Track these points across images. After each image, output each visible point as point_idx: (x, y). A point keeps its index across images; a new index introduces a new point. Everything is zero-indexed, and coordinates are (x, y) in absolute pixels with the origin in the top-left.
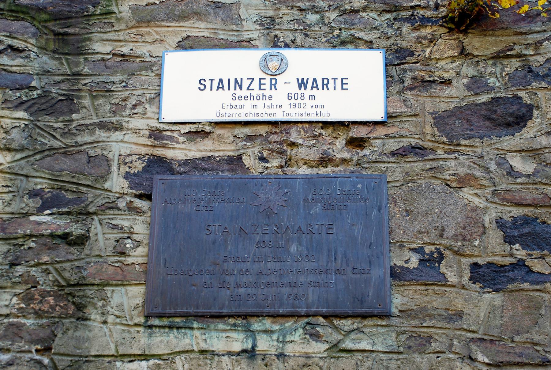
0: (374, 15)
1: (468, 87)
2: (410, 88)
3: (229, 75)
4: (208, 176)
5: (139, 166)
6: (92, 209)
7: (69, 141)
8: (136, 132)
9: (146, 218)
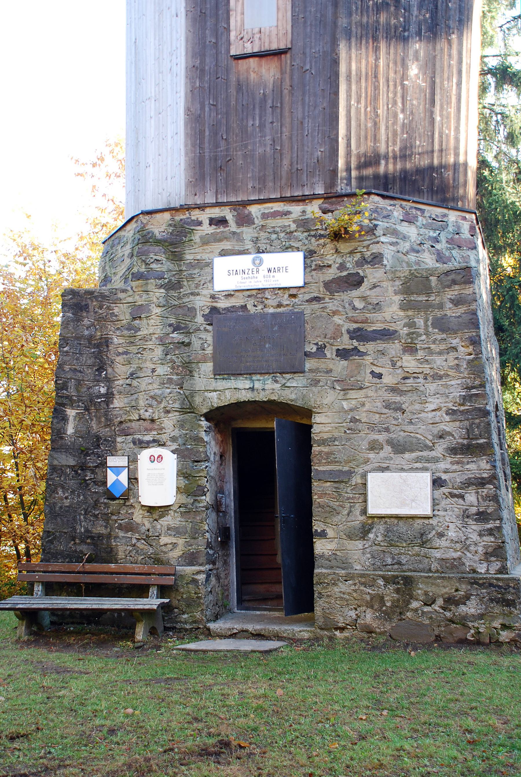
0: (299, 234)
1: (338, 269)
2: (314, 270)
3: (239, 268)
4: (234, 314)
5: (207, 311)
6: (191, 331)
7: (181, 302)
8: (205, 296)
9: (211, 334)
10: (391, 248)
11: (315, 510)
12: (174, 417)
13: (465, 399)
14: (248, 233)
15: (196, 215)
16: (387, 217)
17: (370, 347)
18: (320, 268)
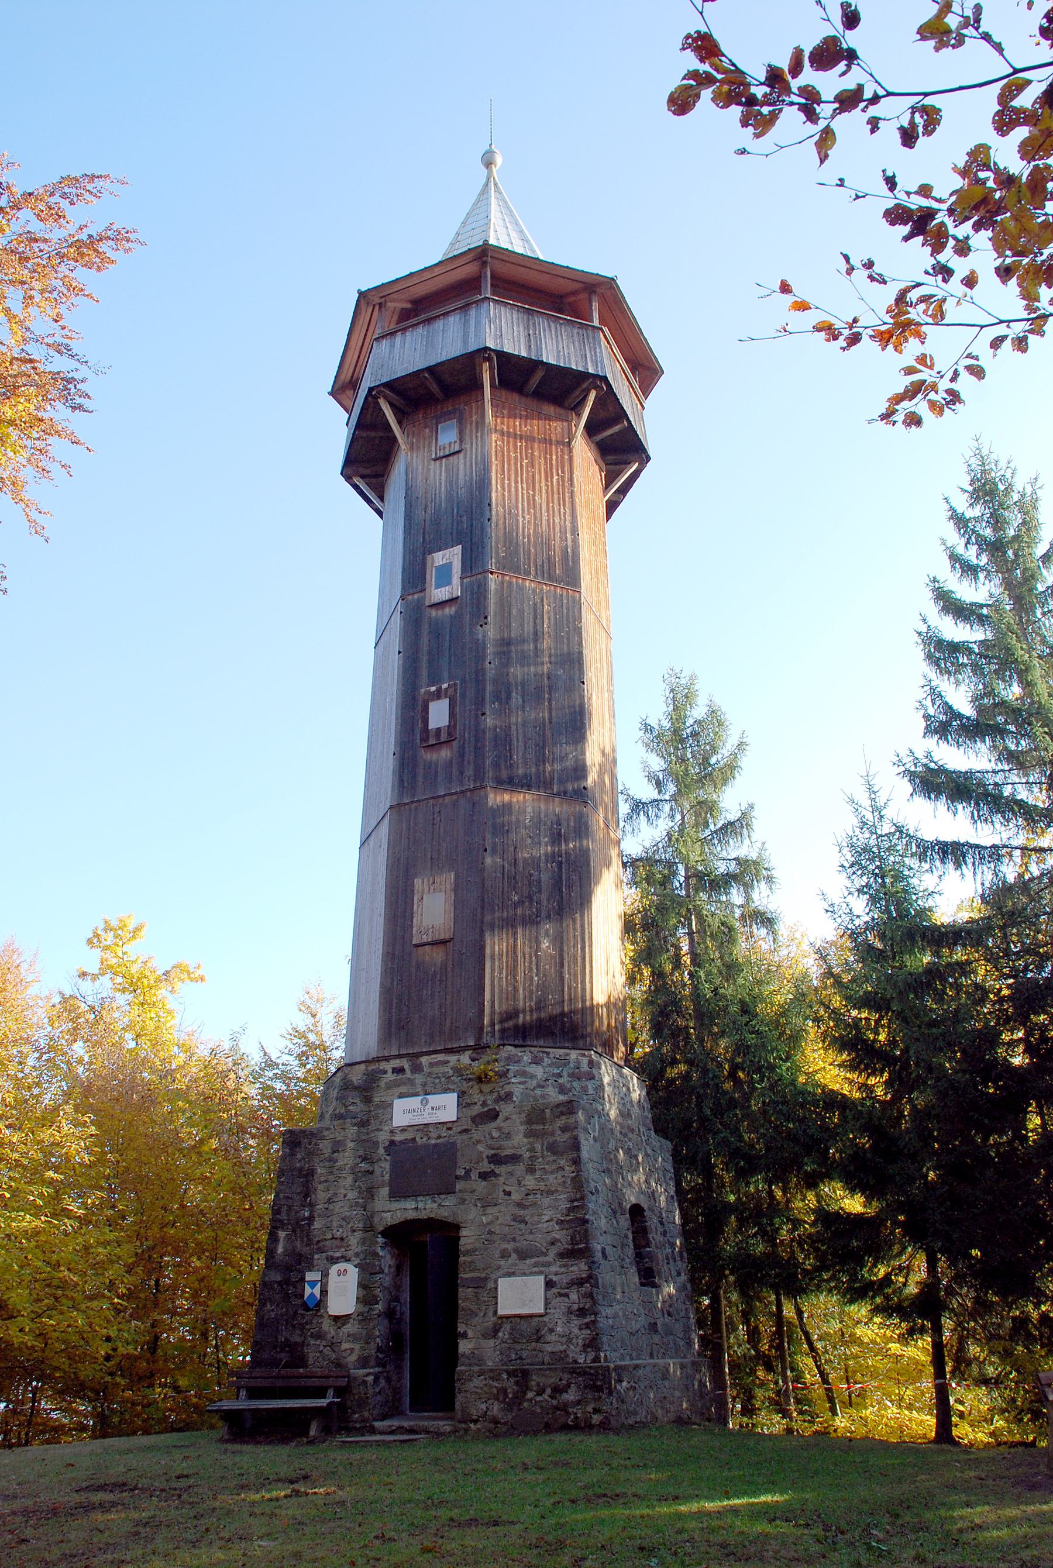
3: (412, 1108)
10: (522, 1086)
11: (460, 1313)
12: (359, 1235)
13: (570, 1210)
14: (419, 1078)
15: (383, 1065)
16: (518, 1061)
17: (502, 1170)
18: (469, 1105)
